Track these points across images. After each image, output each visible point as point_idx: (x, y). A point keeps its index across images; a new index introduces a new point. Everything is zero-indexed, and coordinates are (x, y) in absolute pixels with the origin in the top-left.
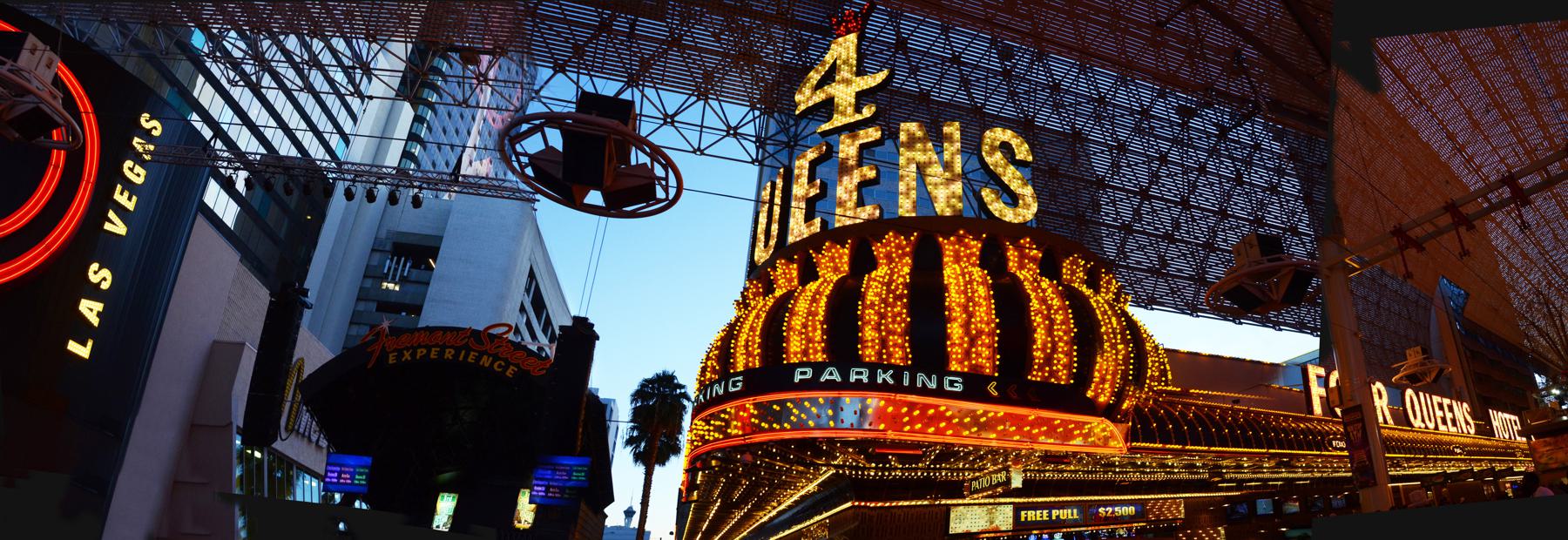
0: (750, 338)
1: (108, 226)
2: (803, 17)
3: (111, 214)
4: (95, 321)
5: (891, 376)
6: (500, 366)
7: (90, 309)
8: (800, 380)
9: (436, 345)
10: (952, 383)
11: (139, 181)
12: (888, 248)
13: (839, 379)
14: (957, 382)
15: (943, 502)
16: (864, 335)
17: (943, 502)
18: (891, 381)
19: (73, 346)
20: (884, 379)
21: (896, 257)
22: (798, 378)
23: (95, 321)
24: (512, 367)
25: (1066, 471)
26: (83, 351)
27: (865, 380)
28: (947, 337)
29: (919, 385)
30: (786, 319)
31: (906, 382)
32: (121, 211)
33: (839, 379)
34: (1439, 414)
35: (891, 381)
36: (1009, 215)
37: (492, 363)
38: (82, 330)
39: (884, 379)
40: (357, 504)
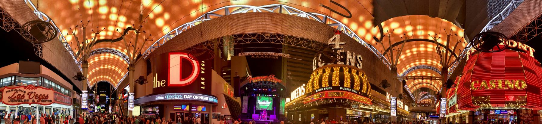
1: (202, 73)
3: (202, 71)
4: (204, 84)
7: (203, 83)
11: (204, 66)
15: (345, 108)
17: (345, 108)
19: (202, 88)
21: (476, 102)
23: (204, 84)
25: (83, 116)
26: (204, 88)
30: (203, 69)
32: (203, 70)
36: (359, 67)
38: (203, 86)
40: (282, 89)
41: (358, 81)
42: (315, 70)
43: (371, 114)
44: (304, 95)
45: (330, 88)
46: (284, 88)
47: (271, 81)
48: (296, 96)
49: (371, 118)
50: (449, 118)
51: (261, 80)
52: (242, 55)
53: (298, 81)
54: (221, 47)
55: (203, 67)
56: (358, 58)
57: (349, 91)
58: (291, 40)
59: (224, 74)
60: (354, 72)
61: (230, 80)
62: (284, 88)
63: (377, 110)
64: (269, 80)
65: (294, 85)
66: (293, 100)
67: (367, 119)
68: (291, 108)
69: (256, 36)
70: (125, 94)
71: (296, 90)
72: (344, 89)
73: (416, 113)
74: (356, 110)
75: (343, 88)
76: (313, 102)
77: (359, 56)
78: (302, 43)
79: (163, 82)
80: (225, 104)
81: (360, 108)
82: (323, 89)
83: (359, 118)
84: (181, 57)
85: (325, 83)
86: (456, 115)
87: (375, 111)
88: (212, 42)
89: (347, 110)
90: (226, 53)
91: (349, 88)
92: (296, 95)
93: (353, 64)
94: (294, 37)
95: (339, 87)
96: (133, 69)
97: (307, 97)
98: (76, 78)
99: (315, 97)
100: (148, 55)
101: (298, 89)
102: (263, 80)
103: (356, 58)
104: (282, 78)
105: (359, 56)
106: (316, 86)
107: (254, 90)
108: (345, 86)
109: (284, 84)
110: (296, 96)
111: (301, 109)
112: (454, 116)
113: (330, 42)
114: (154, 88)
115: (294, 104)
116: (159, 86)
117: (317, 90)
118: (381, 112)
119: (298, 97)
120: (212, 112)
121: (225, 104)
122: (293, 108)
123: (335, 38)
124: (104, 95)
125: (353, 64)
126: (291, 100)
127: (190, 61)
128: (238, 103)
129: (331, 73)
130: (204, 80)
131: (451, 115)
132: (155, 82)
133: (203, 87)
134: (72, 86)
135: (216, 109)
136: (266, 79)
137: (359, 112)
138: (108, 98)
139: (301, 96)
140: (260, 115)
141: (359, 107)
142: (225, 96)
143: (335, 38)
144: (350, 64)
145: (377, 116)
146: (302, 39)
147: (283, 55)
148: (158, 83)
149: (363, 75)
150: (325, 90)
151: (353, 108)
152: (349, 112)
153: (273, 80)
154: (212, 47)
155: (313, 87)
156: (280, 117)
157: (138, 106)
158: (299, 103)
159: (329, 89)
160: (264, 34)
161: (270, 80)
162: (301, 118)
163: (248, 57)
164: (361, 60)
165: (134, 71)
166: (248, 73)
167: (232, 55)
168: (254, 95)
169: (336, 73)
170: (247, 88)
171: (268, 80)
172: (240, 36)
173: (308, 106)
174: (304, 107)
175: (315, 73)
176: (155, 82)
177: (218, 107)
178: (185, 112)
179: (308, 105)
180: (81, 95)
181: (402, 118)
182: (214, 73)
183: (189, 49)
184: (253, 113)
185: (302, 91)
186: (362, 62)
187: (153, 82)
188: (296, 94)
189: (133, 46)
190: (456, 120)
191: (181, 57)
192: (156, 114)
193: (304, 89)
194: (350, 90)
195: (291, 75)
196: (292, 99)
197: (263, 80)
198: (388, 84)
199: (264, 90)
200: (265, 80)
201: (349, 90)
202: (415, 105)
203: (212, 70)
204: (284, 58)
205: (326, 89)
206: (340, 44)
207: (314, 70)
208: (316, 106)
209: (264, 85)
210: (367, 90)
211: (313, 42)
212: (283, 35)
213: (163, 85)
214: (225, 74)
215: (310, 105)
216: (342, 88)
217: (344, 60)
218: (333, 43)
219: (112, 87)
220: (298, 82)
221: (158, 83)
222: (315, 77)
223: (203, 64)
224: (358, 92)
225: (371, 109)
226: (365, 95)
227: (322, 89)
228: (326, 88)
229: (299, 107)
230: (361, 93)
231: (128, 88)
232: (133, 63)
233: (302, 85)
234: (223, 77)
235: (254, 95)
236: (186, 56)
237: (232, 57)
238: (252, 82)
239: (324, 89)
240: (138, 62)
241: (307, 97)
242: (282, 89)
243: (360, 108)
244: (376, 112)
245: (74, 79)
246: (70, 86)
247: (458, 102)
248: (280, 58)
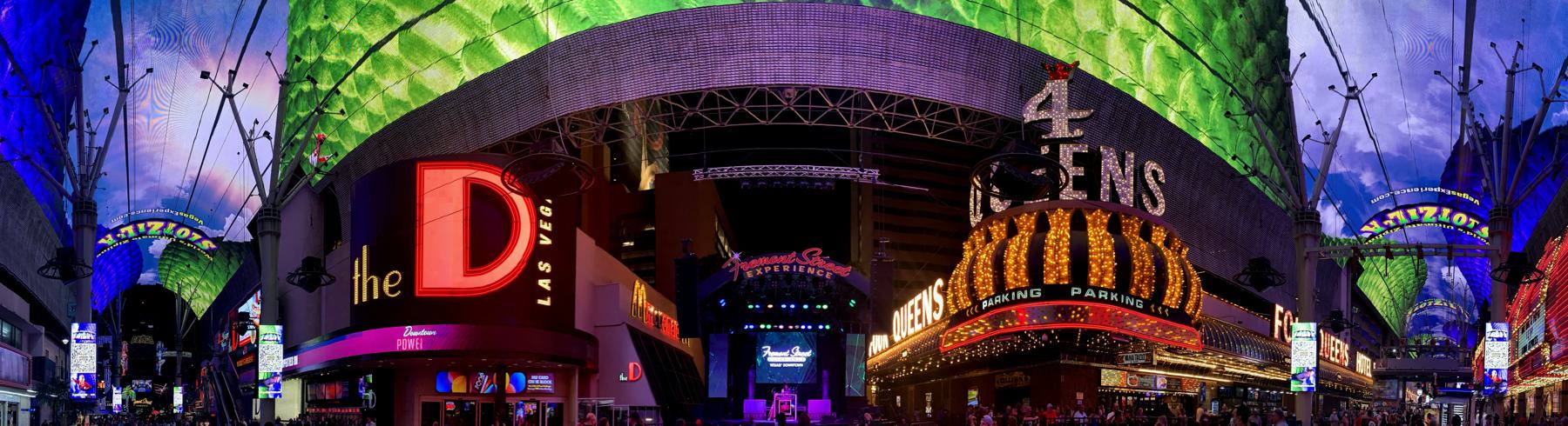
1: (542, 242)
3: (542, 236)
4: (548, 288)
6: (821, 273)
7: (544, 284)
9: (776, 264)
11: (549, 215)
19: (540, 302)
22: (1073, 293)
23: (548, 288)
24: (775, 267)
26: (547, 303)
30: (547, 227)
34: (1332, 349)
37: (815, 271)
38: (543, 294)
40: (853, 302)
41: (1148, 264)
42: (979, 225)
43: (1204, 383)
44: (940, 323)
45: (1034, 293)
46: (861, 298)
47: (811, 271)
48: (913, 325)
49: (1204, 399)
50: (1522, 397)
51: (773, 269)
52: (706, 175)
53: (919, 265)
54: (614, 137)
55: (546, 219)
56: (1148, 176)
57: (1109, 301)
58: (881, 112)
59: (627, 244)
60: (1132, 232)
61: (653, 268)
62: (861, 298)
63: (1227, 369)
64: (801, 269)
65: (903, 284)
66: (900, 343)
67: (1190, 404)
68: (894, 372)
69: (746, 102)
70: (243, 331)
71: (911, 303)
72: (1087, 294)
73: (1401, 383)
74: (1141, 370)
75: (1084, 292)
76: (972, 347)
77: (1151, 166)
78: (926, 121)
79: (393, 279)
80: (634, 365)
81: (1155, 363)
82: (1010, 297)
83: (1159, 398)
84: (466, 180)
85: (1016, 274)
86: (1548, 386)
87: (1222, 374)
88: (576, 121)
89: (1104, 372)
90: (633, 160)
91: (1109, 291)
92: (913, 322)
93: (1127, 198)
94: (892, 98)
95: (1068, 288)
96: (276, 230)
97: (950, 326)
98: (51, 272)
99: (978, 329)
100: (329, 168)
101: (918, 298)
102: (781, 268)
103: (1139, 172)
104: (854, 257)
105: (1151, 166)
106: (984, 277)
107: (751, 307)
108: (1093, 281)
109: (865, 281)
110: (913, 325)
111: (932, 373)
112: (1542, 388)
113: (1030, 114)
114: (356, 302)
115: (905, 354)
116: (376, 297)
117: (987, 299)
118: (1250, 376)
119: (918, 327)
120: (1076, 149)
121: (631, 365)
122: (901, 370)
123: (1051, 95)
124: (148, 340)
125: (1127, 198)
126: (892, 343)
127: (501, 198)
128: (692, 358)
129: (1039, 236)
130: (548, 271)
131: (1527, 388)
132: (360, 279)
133: (545, 299)
134: (27, 306)
135: (593, 387)
136: (791, 266)
137: (1155, 377)
138: (167, 354)
139: (931, 327)
140: (769, 404)
141: (1152, 360)
142: (631, 329)
143: (1051, 95)
144: (1115, 196)
145: (1233, 392)
146: (923, 105)
147: (854, 174)
148: (370, 284)
149: (1167, 243)
150: (1017, 302)
151: (1126, 362)
152: (1110, 378)
153: (816, 267)
154: (576, 140)
155: (972, 292)
156: (848, 407)
157: (291, 378)
158: (928, 349)
159: (1032, 296)
160: (780, 89)
161: (806, 269)
162: (933, 405)
163: (724, 185)
164: (1159, 183)
165: (278, 235)
166: (722, 239)
167: (662, 168)
168: (752, 327)
169: (1059, 233)
170: (723, 303)
171: (798, 268)
172: (691, 98)
173: (955, 361)
174: (942, 364)
175: (978, 238)
176: (360, 279)
177: (598, 376)
178: (481, 400)
179: (956, 358)
180: (65, 341)
181: (1347, 401)
182: (585, 244)
183: (498, 148)
184: (747, 397)
185: (935, 306)
186: (1163, 191)
187: (352, 282)
188: (911, 317)
189: (269, 138)
190: (1549, 402)
191: (466, 180)
192: (362, 410)
193: (939, 299)
194: (1114, 297)
195: (892, 246)
196: (897, 338)
197: (781, 268)
198: (1277, 273)
199: (784, 306)
200: (786, 268)
201: (1109, 296)
202: (1398, 354)
203: (578, 230)
204: (859, 184)
205: (1018, 297)
206: (1069, 120)
207: (973, 225)
208: (991, 356)
209: (785, 289)
210: (1185, 298)
211: (965, 113)
212: (850, 93)
213: (392, 290)
214: (630, 247)
215: (963, 356)
216: (1079, 292)
217: (1089, 184)
218: (1043, 115)
219: (185, 304)
220: (919, 273)
221: (370, 284)
222: (977, 253)
223: (548, 209)
224: (1146, 302)
225: (1203, 368)
226: (1179, 316)
227: (1005, 297)
228: (1020, 294)
229: (922, 366)
230: (1160, 309)
231: (251, 307)
232: (274, 205)
233: (933, 285)
234: (623, 257)
235: (752, 327)
236: (495, 179)
237: (658, 179)
238: (744, 278)
239: (1013, 298)
240: (293, 198)
241: (950, 326)
242: (852, 303)
243: (1155, 363)
244: (1225, 377)
245: (43, 275)
246: (21, 307)
247: (1549, 339)
248: (843, 185)
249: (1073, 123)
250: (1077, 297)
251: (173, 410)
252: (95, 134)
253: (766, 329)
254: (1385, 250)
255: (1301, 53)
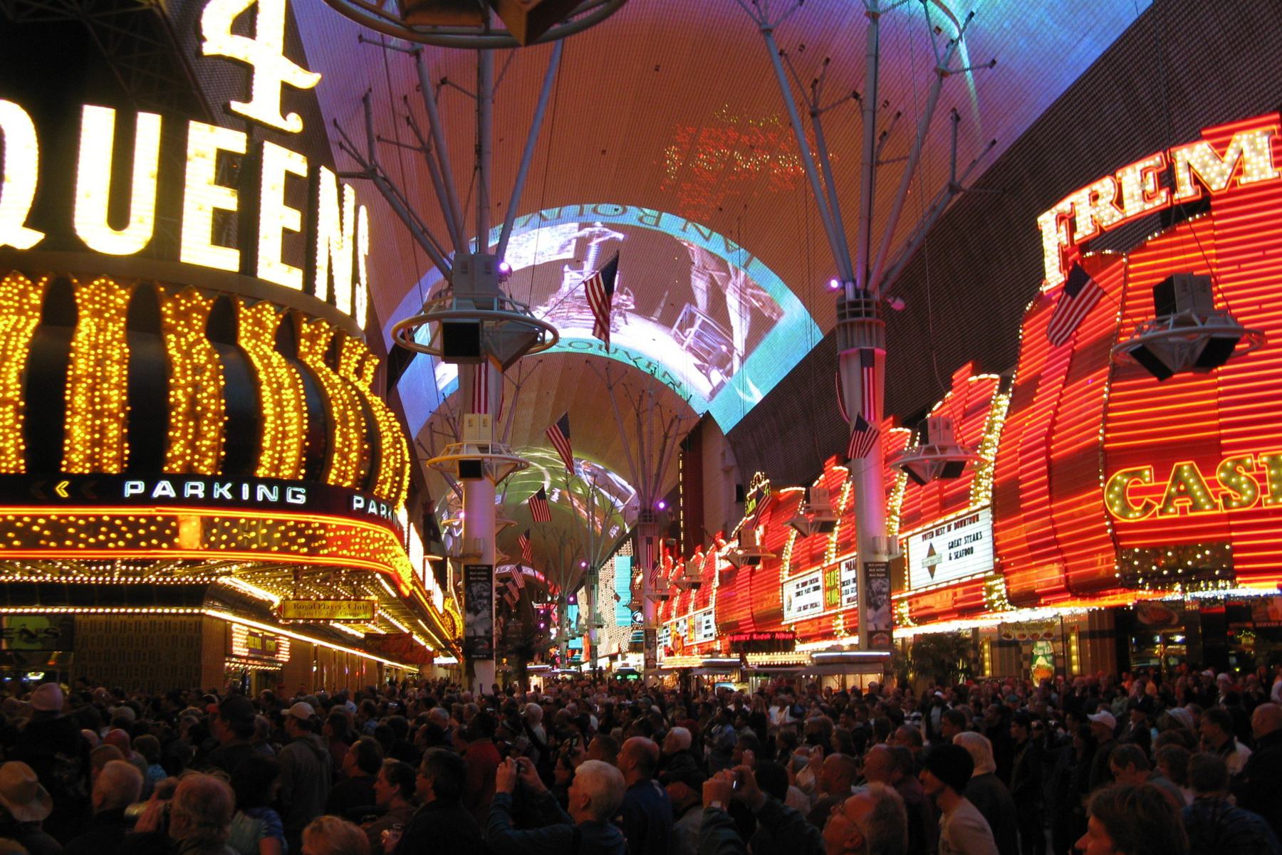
0: (279, 442)
2: (1087, 383)
5: (229, 490)
8: (132, 495)
10: (294, 495)
12: (189, 305)
13: (173, 494)
14: (300, 493)
16: (120, 430)
18: (228, 496)
20: (221, 494)
22: (128, 492)
27: (201, 495)
28: (67, 434)
29: (260, 498)
31: (246, 496)
33: (173, 494)
35: (228, 496)
39: (221, 494)
72: (158, 492)
75: (150, 487)
95: (350, 493)
159: (290, 500)
194: (224, 491)
249: (291, 98)
250: (136, 501)
251: (379, 364)
252: (445, 78)
253: (219, 380)
254: (1238, 468)
255: (357, 40)
